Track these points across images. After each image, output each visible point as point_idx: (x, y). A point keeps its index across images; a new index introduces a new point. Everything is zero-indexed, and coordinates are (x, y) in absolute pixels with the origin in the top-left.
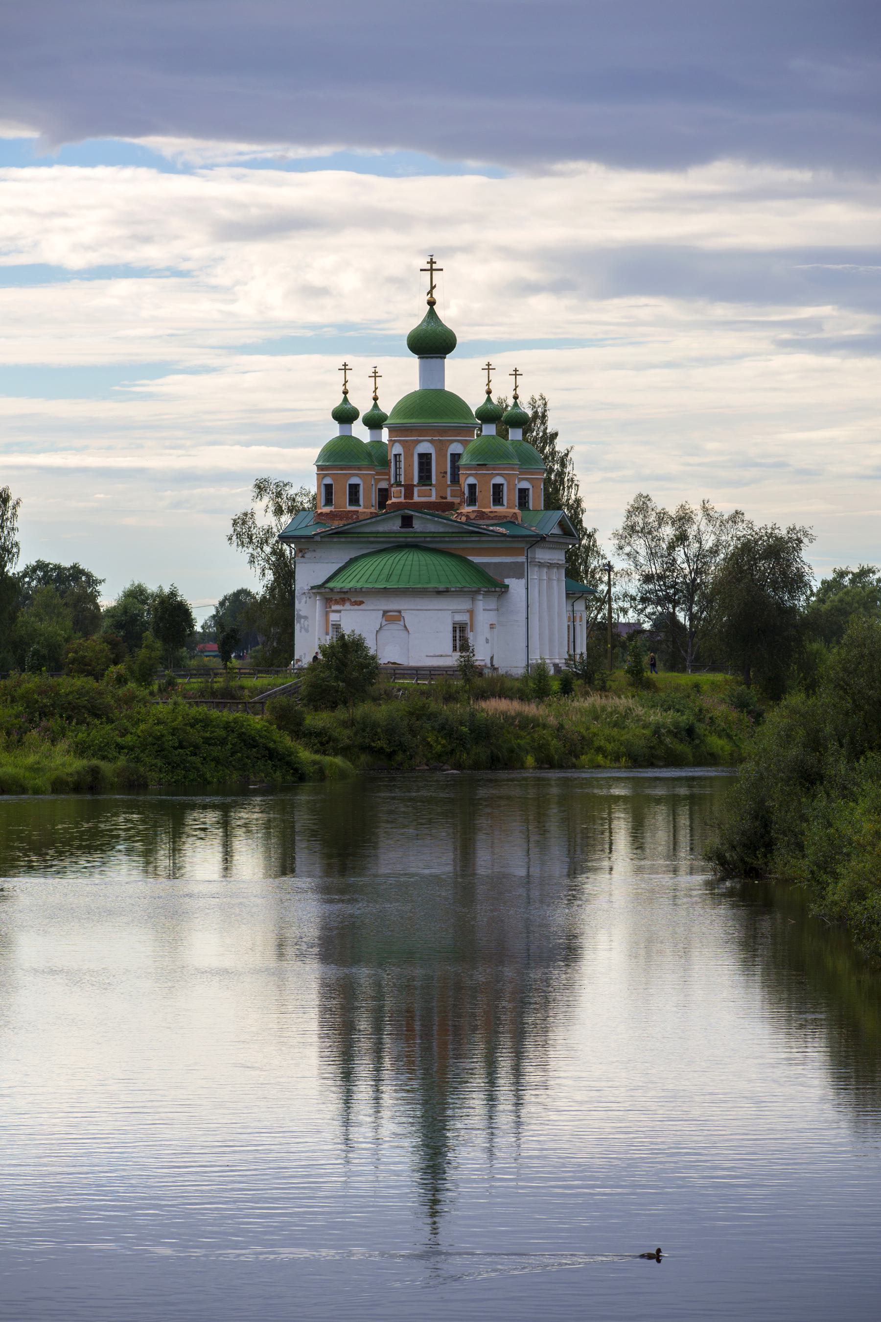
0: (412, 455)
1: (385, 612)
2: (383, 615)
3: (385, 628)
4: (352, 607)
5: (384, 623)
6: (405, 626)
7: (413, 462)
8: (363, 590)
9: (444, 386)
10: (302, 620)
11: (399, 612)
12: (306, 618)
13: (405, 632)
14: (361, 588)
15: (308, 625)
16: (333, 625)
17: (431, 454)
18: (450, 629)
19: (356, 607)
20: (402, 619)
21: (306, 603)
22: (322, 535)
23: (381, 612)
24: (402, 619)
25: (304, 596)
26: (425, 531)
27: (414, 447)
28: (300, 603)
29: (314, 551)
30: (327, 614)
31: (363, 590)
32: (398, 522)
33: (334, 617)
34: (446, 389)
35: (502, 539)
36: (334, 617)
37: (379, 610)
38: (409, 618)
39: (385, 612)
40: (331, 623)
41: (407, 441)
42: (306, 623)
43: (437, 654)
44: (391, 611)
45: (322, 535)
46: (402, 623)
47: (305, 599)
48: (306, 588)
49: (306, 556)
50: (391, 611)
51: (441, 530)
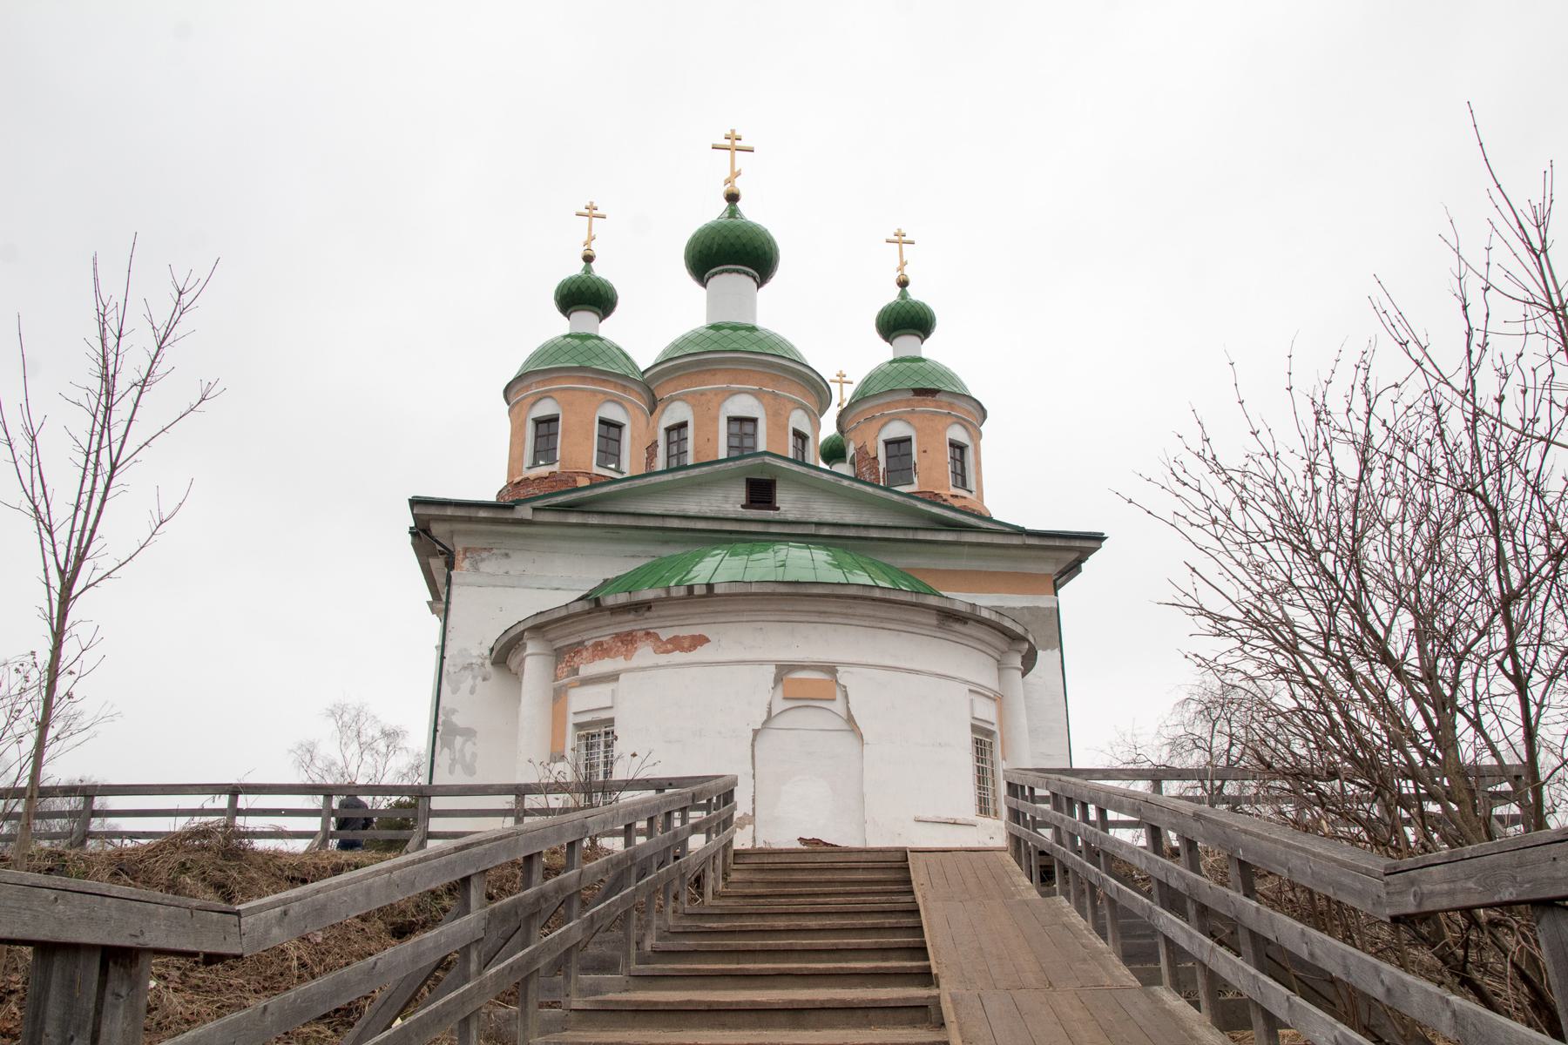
0: (716, 419)
1: (784, 670)
2: (778, 680)
3: (777, 723)
4: (663, 659)
5: (780, 705)
6: (850, 719)
7: (717, 432)
8: (718, 590)
9: (754, 316)
10: (459, 740)
11: (831, 669)
12: (469, 733)
13: (849, 740)
14: (710, 586)
15: (474, 755)
16: (579, 726)
17: (754, 421)
18: (967, 738)
19: (678, 657)
20: (839, 696)
21: (472, 692)
22: (538, 504)
23: (772, 669)
24: (839, 696)
25: (468, 674)
26: (805, 518)
27: (720, 405)
28: (454, 691)
29: (507, 555)
30: (559, 696)
31: (718, 590)
32: (739, 494)
33: (584, 701)
34: (761, 323)
35: (1016, 541)
36: (584, 701)
37: (761, 662)
38: (861, 689)
39: (784, 670)
40: (572, 720)
41: (703, 393)
42: (469, 747)
43: (944, 816)
44: (803, 667)
45: (538, 504)
46: (838, 706)
47: (470, 682)
48: (475, 652)
49: (484, 567)
50: (803, 667)
51: (850, 518)
